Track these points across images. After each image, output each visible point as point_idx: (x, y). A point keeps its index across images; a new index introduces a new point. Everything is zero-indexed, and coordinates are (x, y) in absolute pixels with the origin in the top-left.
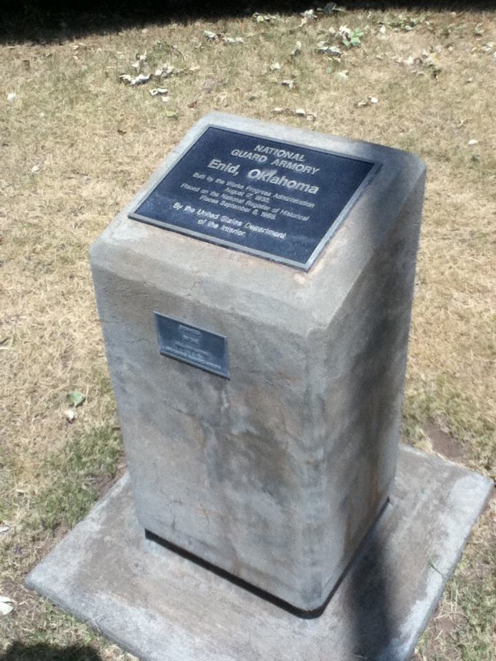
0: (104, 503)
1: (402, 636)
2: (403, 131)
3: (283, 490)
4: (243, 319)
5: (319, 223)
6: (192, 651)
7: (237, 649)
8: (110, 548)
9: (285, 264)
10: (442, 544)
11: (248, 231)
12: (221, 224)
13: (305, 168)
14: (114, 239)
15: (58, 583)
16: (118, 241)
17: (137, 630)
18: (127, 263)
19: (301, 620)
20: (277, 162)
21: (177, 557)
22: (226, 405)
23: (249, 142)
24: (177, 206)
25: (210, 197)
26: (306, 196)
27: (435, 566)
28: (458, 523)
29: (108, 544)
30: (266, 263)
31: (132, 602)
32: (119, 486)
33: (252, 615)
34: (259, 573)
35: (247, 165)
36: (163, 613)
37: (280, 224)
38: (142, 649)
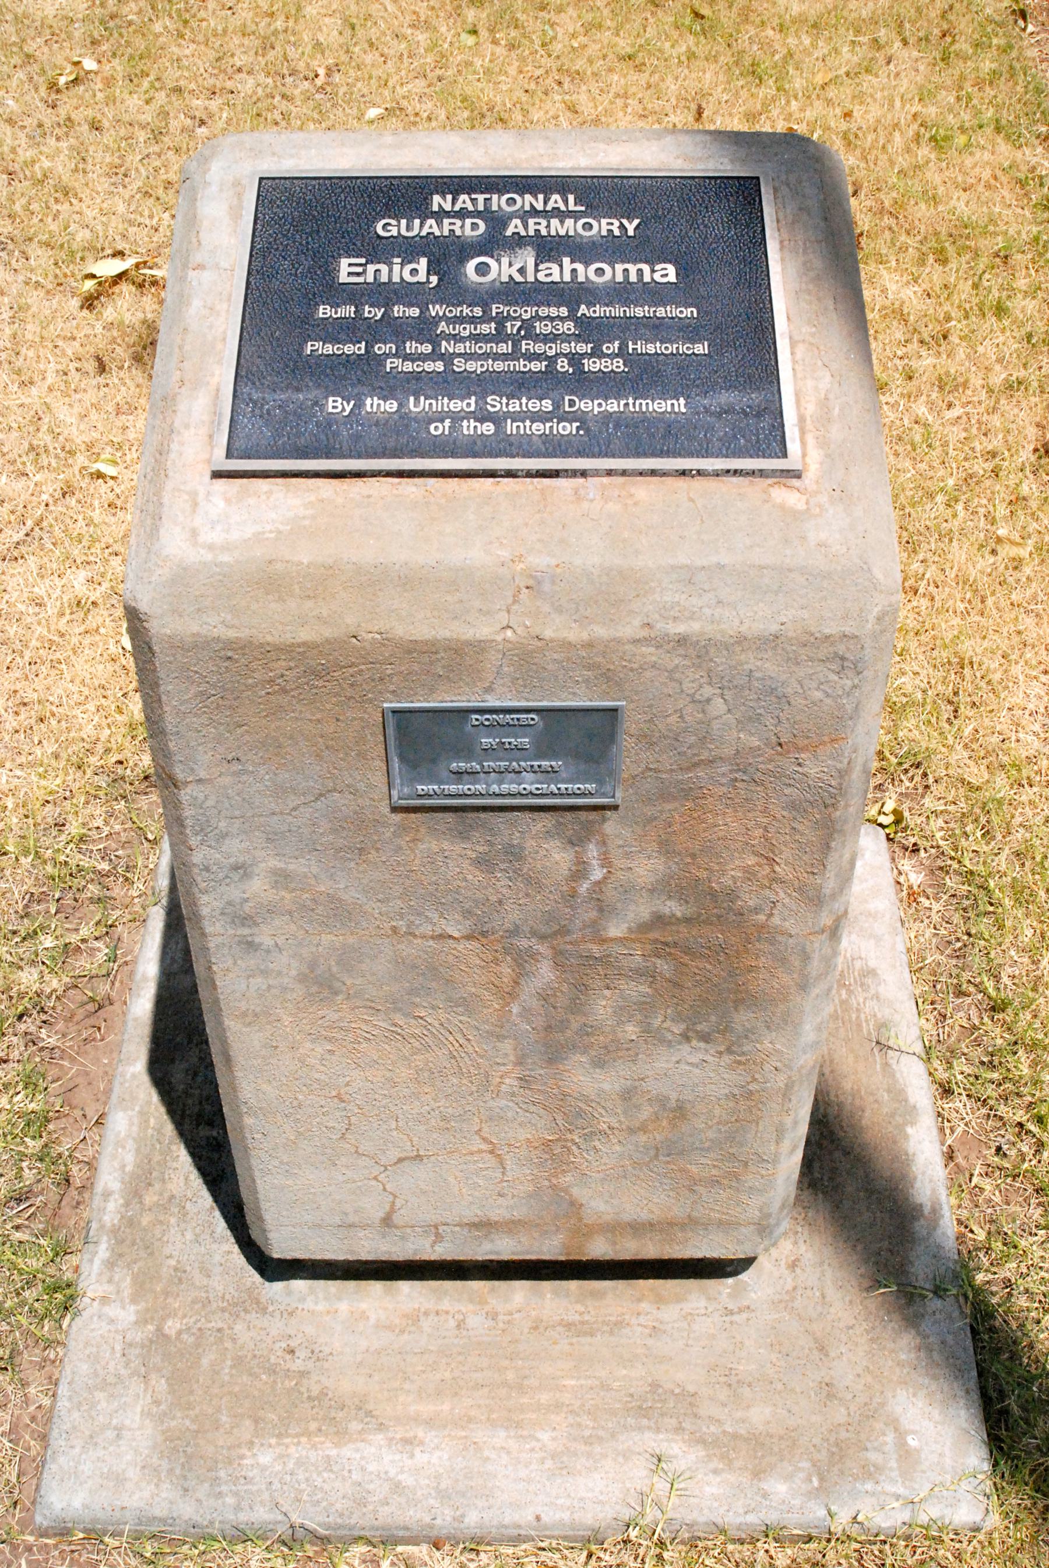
0: (103, 1251)
1: (927, 1210)
2: (202, 123)
3: (742, 1018)
4: (682, 641)
5: (748, 344)
6: (549, 1464)
7: (640, 1407)
8: (198, 1345)
9: (736, 472)
10: (877, 997)
11: (581, 418)
12: (497, 419)
13: (604, 226)
14: (211, 547)
15: (129, 1485)
16: (226, 548)
17: (397, 1487)
18: (281, 600)
19: (730, 1281)
20: (514, 226)
21: (376, 1287)
22: (597, 874)
23: (409, 194)
24: (336, 405)
25: (407, 357)
26: (656, 294)
27: (891, 1043)
28: (878, 939)
29: (185, 1336)
30: (681, 483)
31: (341, 1436)
32: (107, 1195)
33: (619, 1324)
34: (638, 1228)
35: (446, 255)
36: (430, 1423)
37: (645, 376)
38: (438, 1522)
